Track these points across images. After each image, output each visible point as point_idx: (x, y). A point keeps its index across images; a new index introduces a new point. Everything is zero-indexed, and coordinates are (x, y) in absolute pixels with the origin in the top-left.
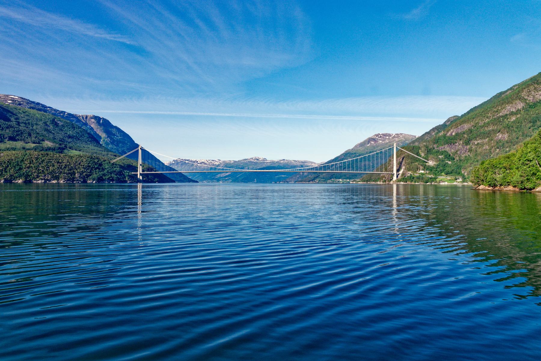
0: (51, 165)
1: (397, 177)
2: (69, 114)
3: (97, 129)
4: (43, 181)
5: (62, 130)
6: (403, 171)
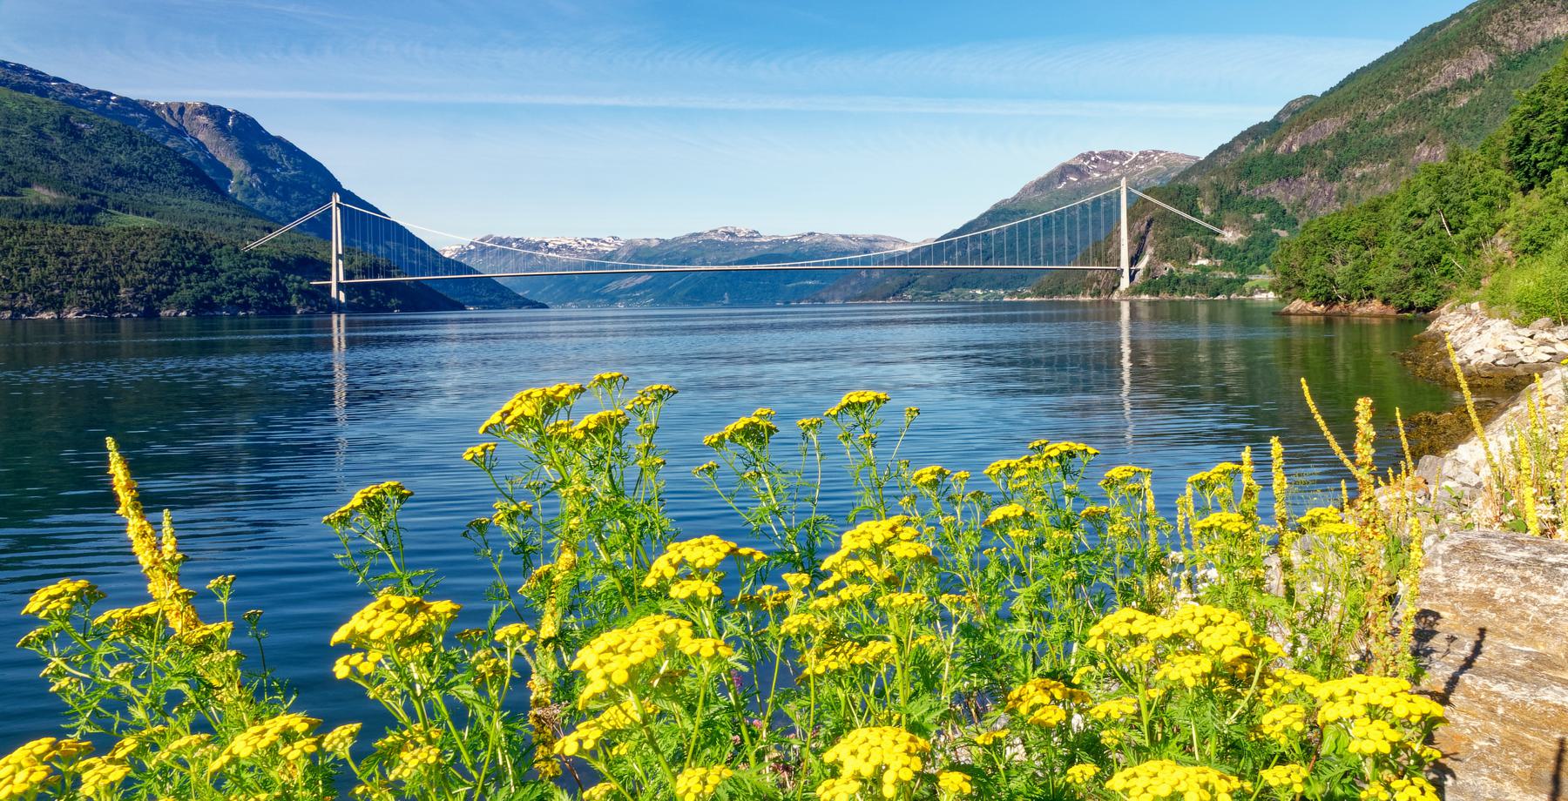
1: (1132, 278)
2: (124, 101)
3: (218, 145)
5: (93, 151)
6: (1149, 262)
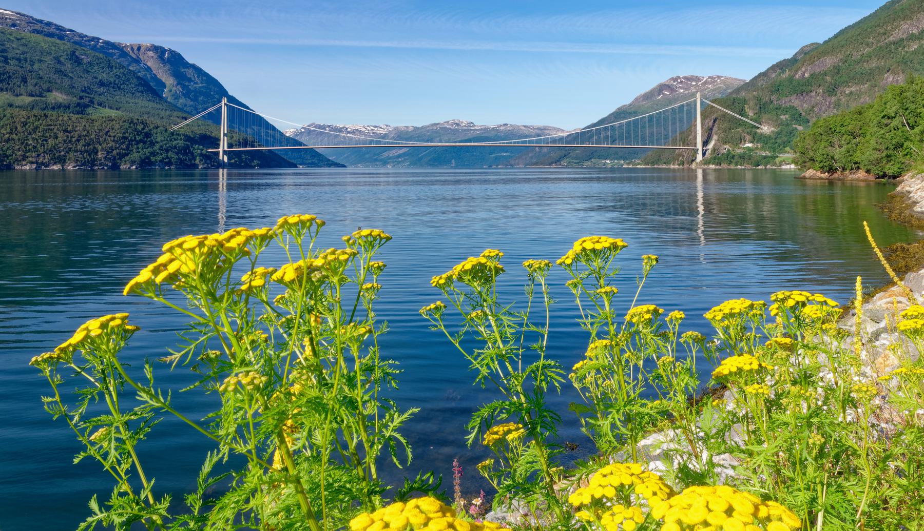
0: (50, 137)
1: (704, 154)
2: (107, 43)
4: (34, 166)
6: (715, 145)
